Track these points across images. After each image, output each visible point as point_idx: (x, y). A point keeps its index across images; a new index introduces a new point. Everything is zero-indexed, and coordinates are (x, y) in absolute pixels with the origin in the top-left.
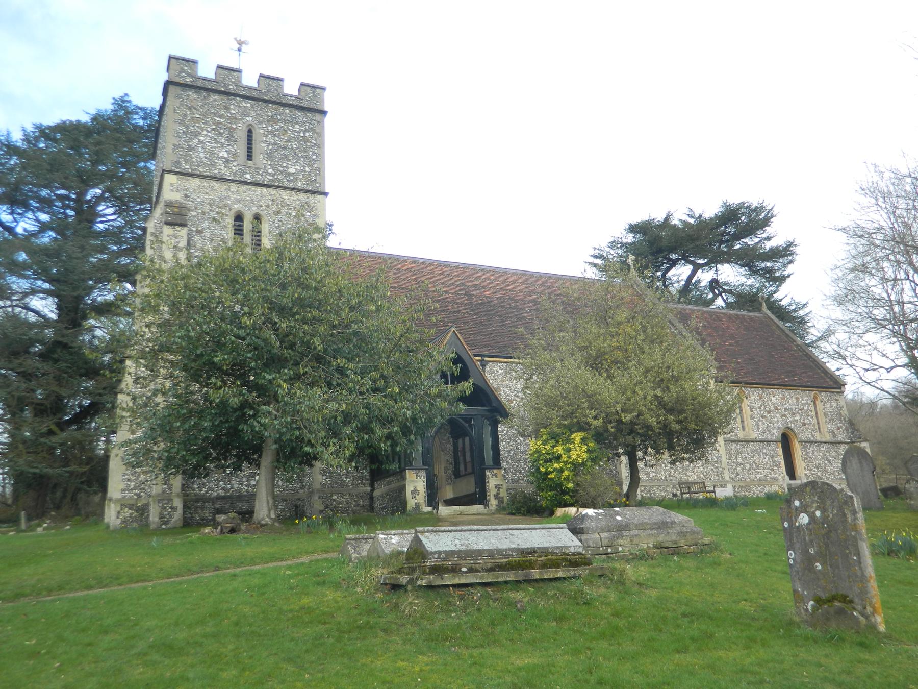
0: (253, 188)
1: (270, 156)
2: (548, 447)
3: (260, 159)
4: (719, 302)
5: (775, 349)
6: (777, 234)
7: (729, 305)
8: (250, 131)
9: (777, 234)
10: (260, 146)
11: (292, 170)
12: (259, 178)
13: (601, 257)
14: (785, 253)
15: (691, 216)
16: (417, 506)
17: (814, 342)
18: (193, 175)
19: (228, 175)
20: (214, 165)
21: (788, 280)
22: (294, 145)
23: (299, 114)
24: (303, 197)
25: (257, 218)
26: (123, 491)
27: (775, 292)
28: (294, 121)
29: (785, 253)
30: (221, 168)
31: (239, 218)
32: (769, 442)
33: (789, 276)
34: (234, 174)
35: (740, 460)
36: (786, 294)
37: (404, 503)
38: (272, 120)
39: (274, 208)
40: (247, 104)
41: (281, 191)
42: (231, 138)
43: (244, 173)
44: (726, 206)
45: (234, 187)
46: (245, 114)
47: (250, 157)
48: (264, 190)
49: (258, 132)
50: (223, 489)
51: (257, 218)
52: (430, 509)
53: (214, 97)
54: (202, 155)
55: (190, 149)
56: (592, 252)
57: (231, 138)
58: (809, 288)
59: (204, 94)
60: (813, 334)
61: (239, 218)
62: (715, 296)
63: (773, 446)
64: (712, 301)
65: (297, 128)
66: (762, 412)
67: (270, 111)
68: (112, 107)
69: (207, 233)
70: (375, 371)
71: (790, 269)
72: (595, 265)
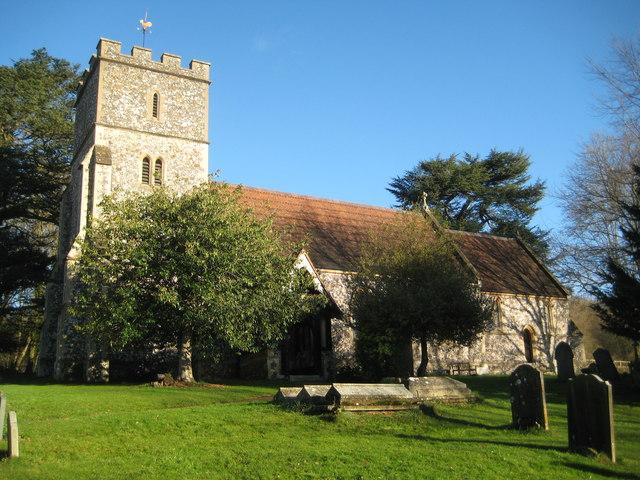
0: (156, 137)
1: (169, 114)
2: (369, 338)
3: (162, 116)
4: (487, 228)
5: (526, 266)
6: (531, 177)
7: (494, 231)
8: (155, 95)
9: (531, 177)
10: (163, 107)
11: (184, 125)
12: (160, 130)
13: (399, 186)
14: (535, 193)
15: (468, 160)
16: (275, 374)
17: (552, 260)
18: (115, 127)
19: (139, 127)
20: (129, 120)
21: (537, 212)
22: (186, 106)
23: (190, 83)
24: (192, 144)
25: (159, 162)
26: (65, 354)
27: (526, 224)
28: (187, 88)
29: (535, 193)
30: (135, 123)
31: (147, 160)
32: (111, 61)
33: (537, 209)
34: (144, 127)
35: (494, 348)
36: (535, 223)
37: (266, 372)
38: (171, 88)
39: (172, 153)
40: (154, 75)
41: (177, 140)
42: (143, 101)
43: (150, 126)
44: (493, 154)
45: (143, 136)
46: (152, 83)
47: (155, 115)
48: (165, 139)
49: (162, 97)
50: (133, 357)
51: (159, 162)
52: (283, 376)
53: (131, 69)
54: (122, 113)
55: (114, 108)
56: (392, 182)
57: (143, 101)
58: (548, 219)
59: (124, 67)
60: (553, 253)
61: (147, 160)
62: (484, 222)
63: (106, 57)
64: (481, 226)
65: (189, 93)
66: (515, 311)
67: (171, 80)
68: (32, 57)
69: (124, 170)
70: (182, 249)
71: (538, 205)
72: (393, 192)
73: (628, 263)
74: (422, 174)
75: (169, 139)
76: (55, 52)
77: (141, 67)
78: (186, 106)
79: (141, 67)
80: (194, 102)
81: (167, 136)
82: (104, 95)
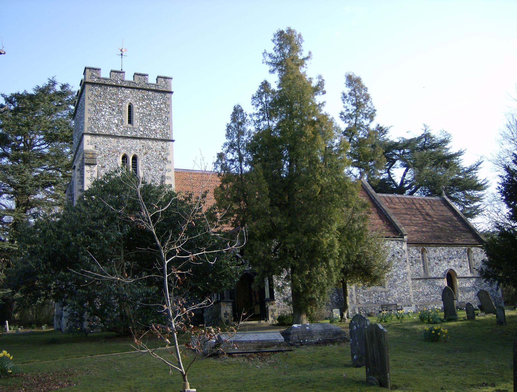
8: (130, 107)
10: (136, 115)
18: (99, 135)
24: (160, 143)
25: (135, 158)
39: (144, 151)
40: (128, 91)
44: (289, 30)
45: (121, 141)
47: (130, 121)
51: (135, 158)
57: (120, 112)
61: (125, 157)
67: (140, 94)
73: (516, 152)
74: (82, 121)
75: (142, 141)
76: (61, 80)
77: (117, 86)
78: (154, 113)
79: (117, 86)
80: (161, 109)
81: (140, 138)
82: (89, 110)
